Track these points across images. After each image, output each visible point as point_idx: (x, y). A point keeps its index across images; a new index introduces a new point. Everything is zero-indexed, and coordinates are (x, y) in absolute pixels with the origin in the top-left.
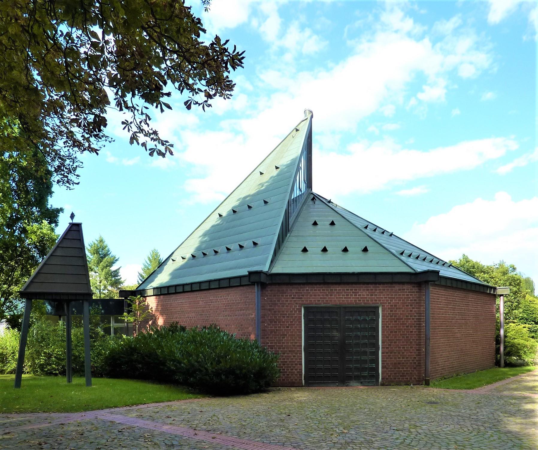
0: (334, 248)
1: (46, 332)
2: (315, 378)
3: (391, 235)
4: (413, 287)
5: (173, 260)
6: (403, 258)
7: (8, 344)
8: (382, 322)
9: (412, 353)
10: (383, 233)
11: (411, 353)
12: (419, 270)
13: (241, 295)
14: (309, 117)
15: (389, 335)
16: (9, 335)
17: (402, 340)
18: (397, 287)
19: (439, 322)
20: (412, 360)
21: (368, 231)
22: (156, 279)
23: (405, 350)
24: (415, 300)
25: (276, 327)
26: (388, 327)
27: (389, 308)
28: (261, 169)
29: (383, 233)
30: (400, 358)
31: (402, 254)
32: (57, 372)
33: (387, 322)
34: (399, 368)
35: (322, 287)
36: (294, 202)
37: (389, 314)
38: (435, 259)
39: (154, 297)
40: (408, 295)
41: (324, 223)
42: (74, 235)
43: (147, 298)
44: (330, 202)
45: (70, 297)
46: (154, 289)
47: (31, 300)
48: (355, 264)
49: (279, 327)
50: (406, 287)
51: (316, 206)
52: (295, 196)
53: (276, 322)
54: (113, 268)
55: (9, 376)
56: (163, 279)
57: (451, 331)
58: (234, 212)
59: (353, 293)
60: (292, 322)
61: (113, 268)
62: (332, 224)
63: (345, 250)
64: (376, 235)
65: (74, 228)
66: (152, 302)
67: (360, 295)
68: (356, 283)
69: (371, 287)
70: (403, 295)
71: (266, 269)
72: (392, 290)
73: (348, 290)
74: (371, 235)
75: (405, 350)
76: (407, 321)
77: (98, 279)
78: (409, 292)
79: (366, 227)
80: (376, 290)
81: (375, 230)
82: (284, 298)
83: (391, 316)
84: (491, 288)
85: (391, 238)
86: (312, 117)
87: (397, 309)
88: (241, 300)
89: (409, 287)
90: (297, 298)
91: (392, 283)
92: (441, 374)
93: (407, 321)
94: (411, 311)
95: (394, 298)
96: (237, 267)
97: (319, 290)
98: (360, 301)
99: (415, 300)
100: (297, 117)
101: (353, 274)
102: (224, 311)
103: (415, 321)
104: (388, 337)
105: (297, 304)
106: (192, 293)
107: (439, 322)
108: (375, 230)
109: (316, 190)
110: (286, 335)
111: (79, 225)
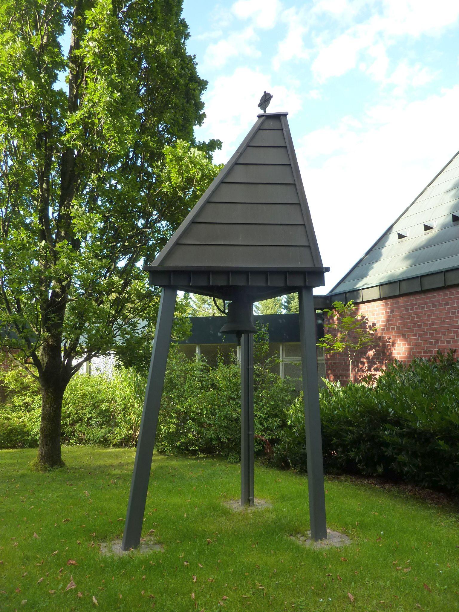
1: (178, 373)
7: (117, 393)
16: (121, 377)
22: (371, 273)
32: (197, 448)
39: (380, 303)
42: (269, 138)
43: (361, 306)
46: (381, 285)
47: (174, 289)
55: (116, 456)
56: (378, 274)
65: (271, 124)
66: (374, 314)
77: (211, 312)
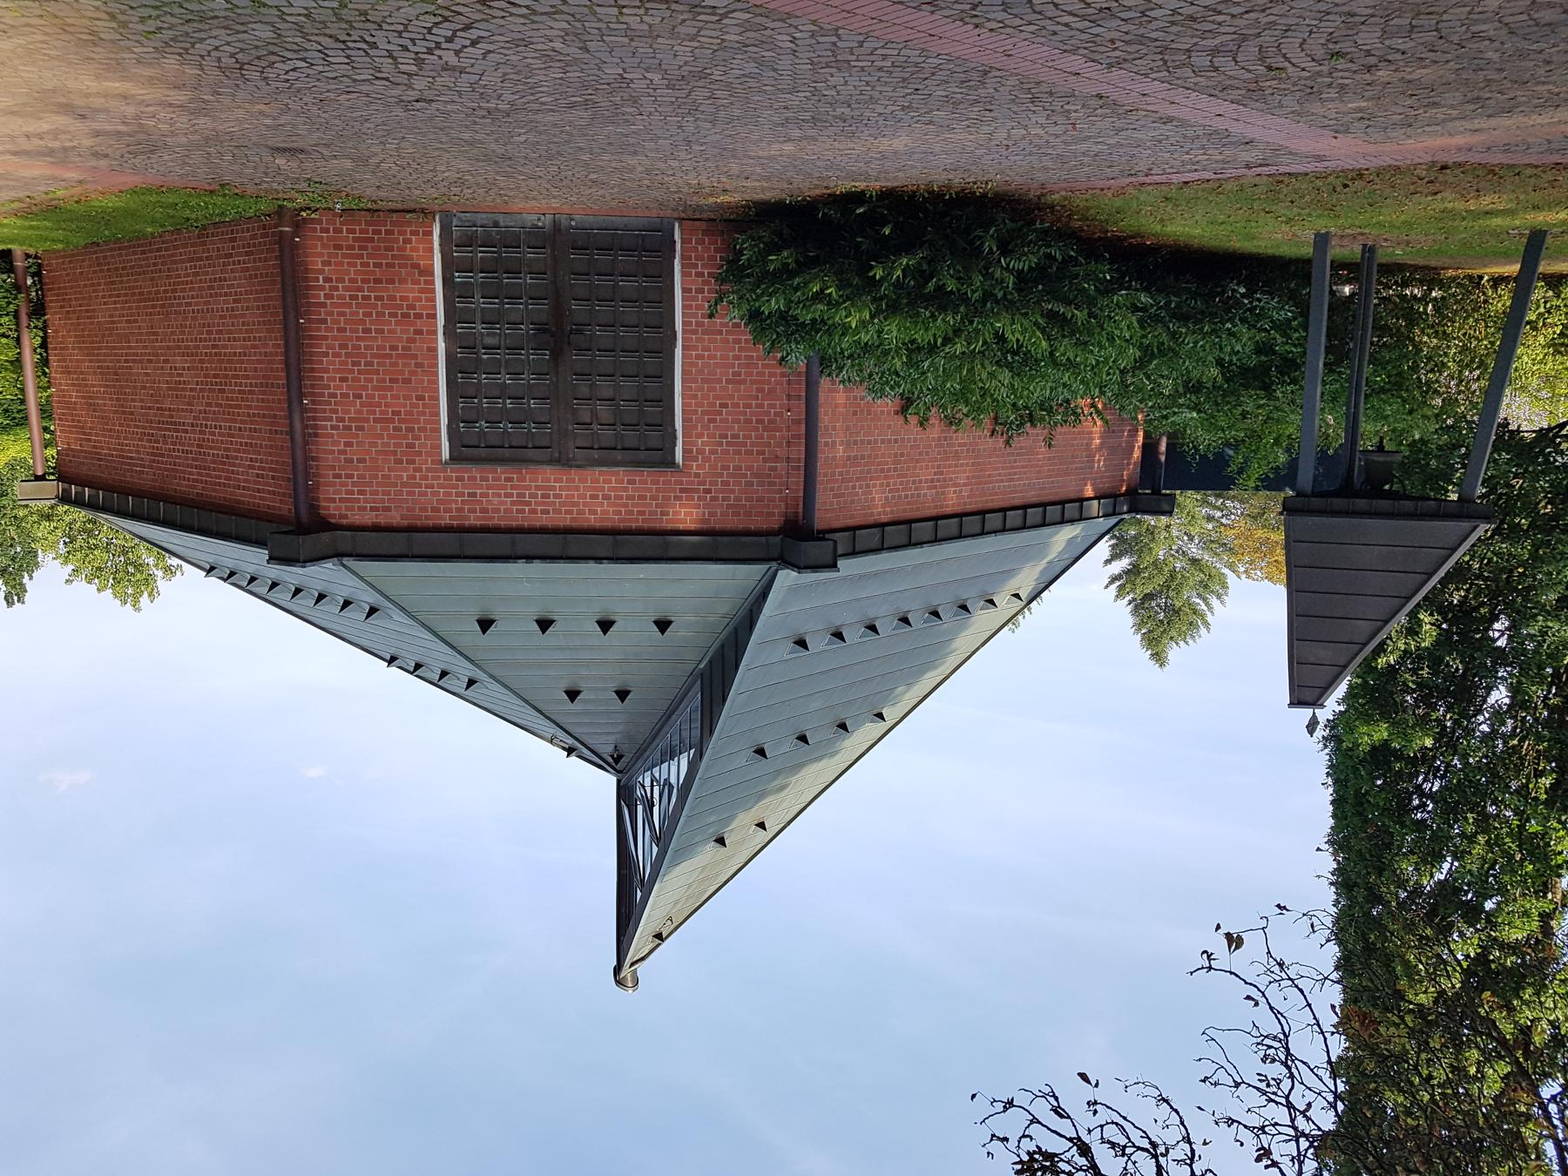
0: (577, 628)
2: (639, 250)
3: (391, 661)
4: (346, 516)
5: (1017, 596)
6: (371, 598)
8: (438, 414)
9: (340, 314)
10: (418, 666)
11: (343, 314)
12: (330, 565)
13: (852, 502)
14: (626, 972)
15: (413, 373)
17: (374, 356)
18: (395, 518)
19: (249, 407)
20: (337, 289)
21: (464, 670)
23: (362, 322)
24: (339, 476)
25: (758, 406)
26: (420, 398)
27: (420, 454)
28: (763, 836)
29: (418, 666)
30: (377, 298)
31: (373, 611)
33: (423, 414)
34: (376, 265)
35: (621, 520)
36: (680, 754)
37: (418, 438)
38: (264, 590)
40: (360, 492)
41: (599, 694)
44: (570, 751)
45: (1339, 503)
48: (520, 586)
49: (749, 406)
50: (368, 518)
51: (612, 739)
52: (674, 764)
53: (759, 421)
54: (1123, 563)
57: (206, 376)
58: (843, 726)
59: (529, 503)
60: (710, 421)
61: (1123, 563)
62: (573, 695)
63: (544, 624)
64: (440, 656)
65: (1308, 695)
67: (507, 495)
68: (520, 530)
69: (473, 520)
70: (376, 493)
71: (786, 578)
72: (409, 509)
73: (546, 512)
74: (463, 666)
75: (362, 322)
76: (361, 412)
78: (358, 500)
79: (471, 682)
80: (460, 510)
81: (444, 674)
82: (733, 491)
83: (411, 430)
84: (78, 502)
85: (393, 651)
86: (617, 970)
87: (395, 453)
88: (854, 487)
89: (356, 518)
90: (697, 491)
91: (411, 529)
92: (233, 240)
93: (361, 412)
94: (347, 444)
95: (404, 485)
96: (866, 584)
97: (631, 512)
98: (507, 480)
99: (339, 476)
100: (656, 969)
101: (529, 558)
102: (902, 455)
103: (336, 412)
104: (417, 365)
105: (697, 475)
106: (980, 506)
107: (249, 407)
108: (444, 674)
109: (607, 782)
110: (728, 382)
111: (1296, 702)
